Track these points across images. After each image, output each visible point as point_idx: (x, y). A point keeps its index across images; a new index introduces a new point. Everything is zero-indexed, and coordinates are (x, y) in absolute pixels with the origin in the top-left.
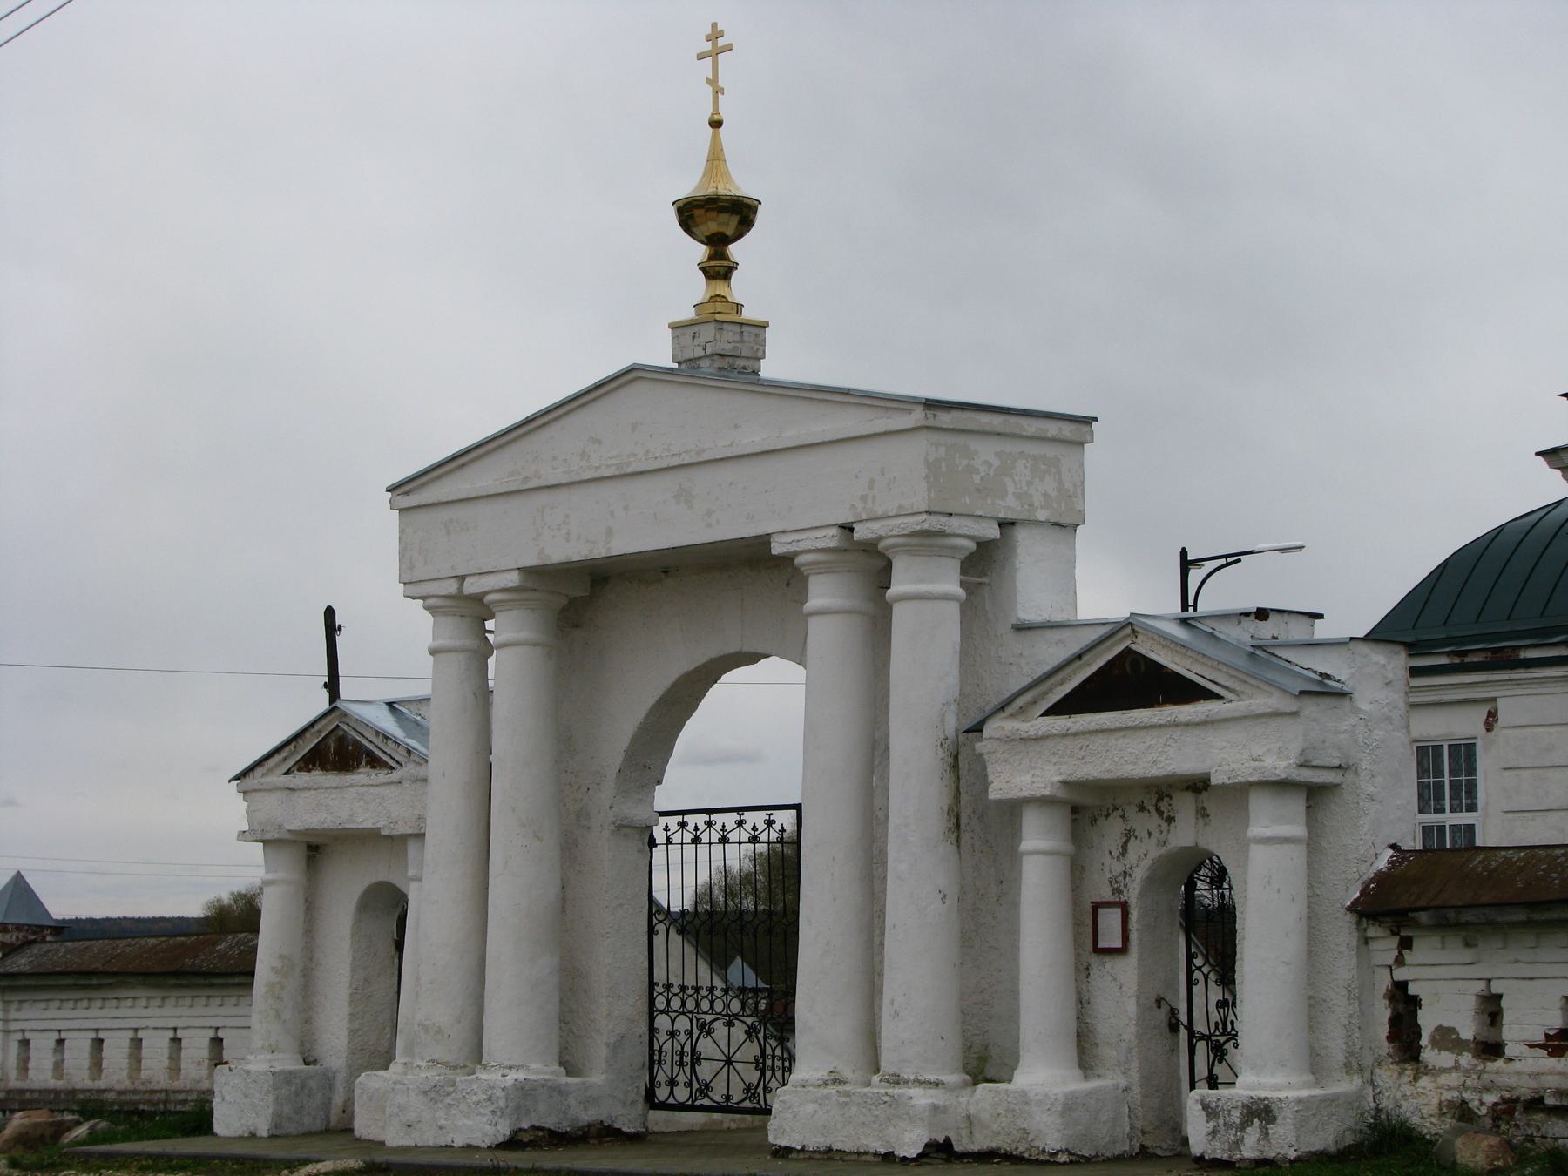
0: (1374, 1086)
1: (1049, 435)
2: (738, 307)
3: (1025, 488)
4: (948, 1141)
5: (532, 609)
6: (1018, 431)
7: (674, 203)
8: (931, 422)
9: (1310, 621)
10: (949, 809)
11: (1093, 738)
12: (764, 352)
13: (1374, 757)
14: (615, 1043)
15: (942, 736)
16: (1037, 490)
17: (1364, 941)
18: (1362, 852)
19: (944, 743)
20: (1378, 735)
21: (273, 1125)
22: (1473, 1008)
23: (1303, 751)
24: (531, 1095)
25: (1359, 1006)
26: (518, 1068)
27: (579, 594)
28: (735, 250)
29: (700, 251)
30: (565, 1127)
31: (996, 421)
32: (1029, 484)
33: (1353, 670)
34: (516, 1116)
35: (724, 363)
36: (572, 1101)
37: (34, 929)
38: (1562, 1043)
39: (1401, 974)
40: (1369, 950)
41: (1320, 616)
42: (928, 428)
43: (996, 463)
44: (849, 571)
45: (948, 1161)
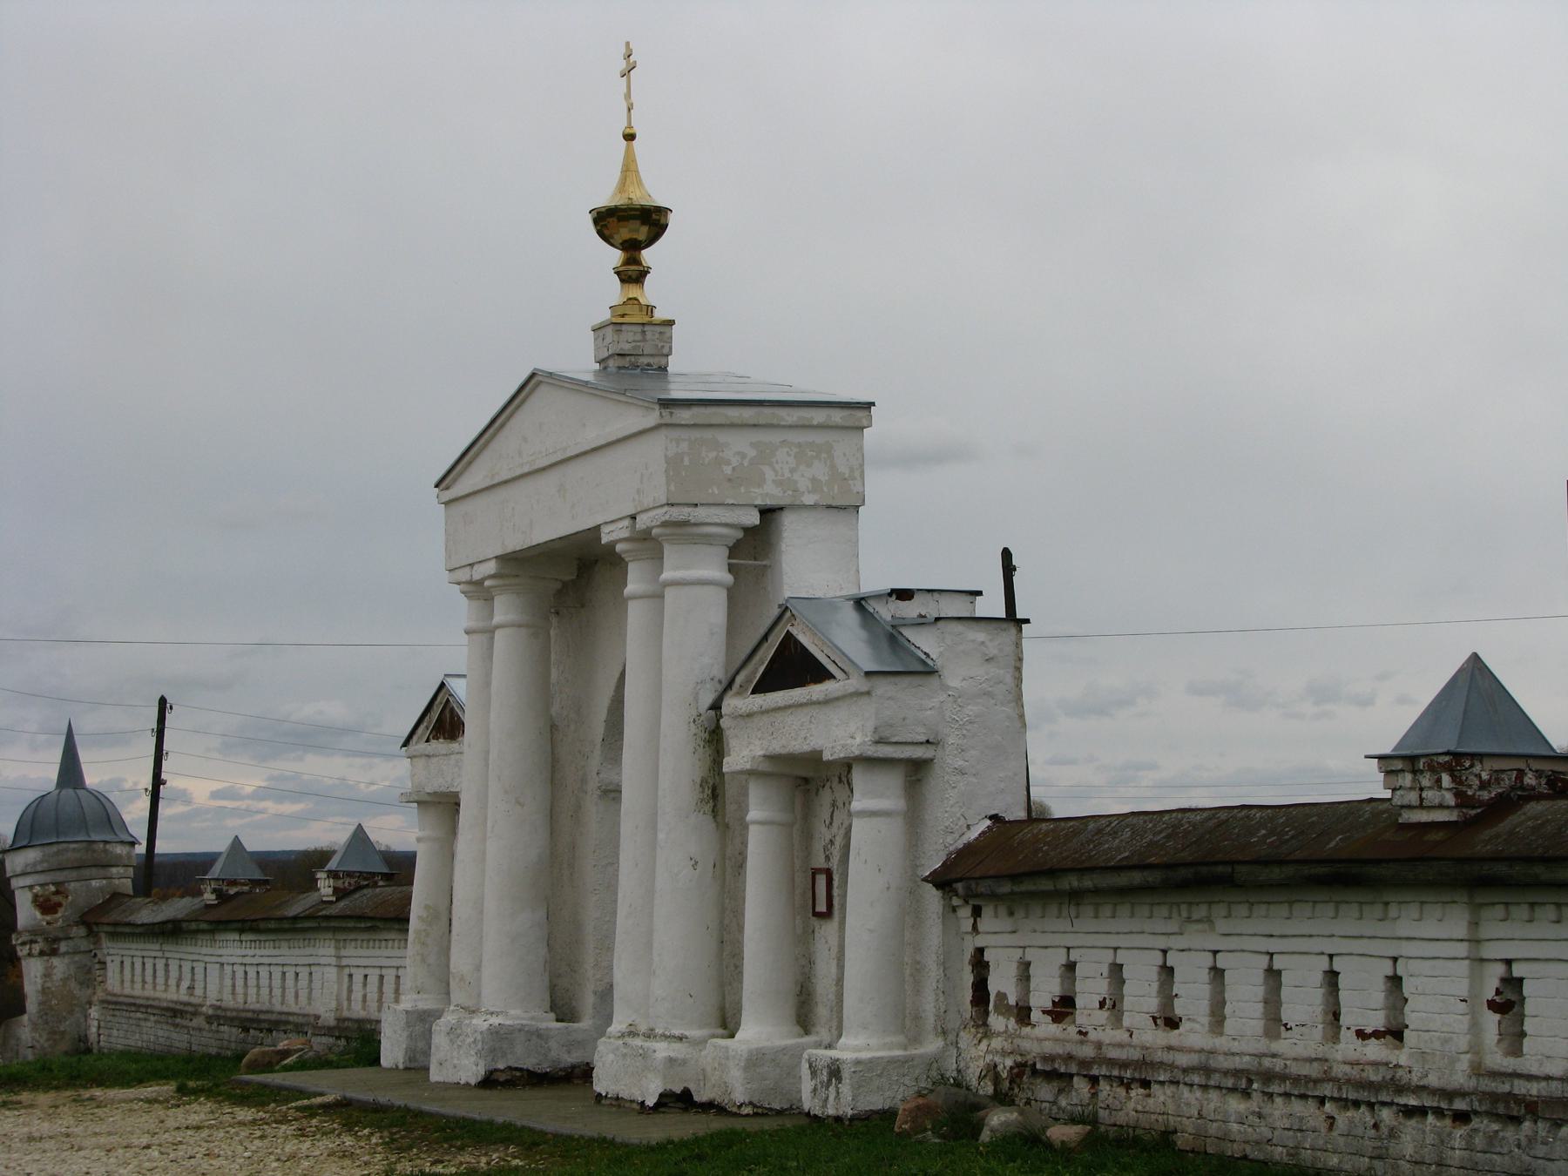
0: (958, 1048)
1: (815, 423)
2: (650, 309)
3: (787, 475)
4: (687, 1094)
5: (518, 593)
6: (775, 422)
7: (590, 212)
8: (667, 420)
9: (970, 598)
10: (702, 781)
11: (777, 715)
12: (671, 348)
13: (965, 732)
14: (602, 991)
15: (695, 713)
16: (803, 476)
17: (951, 910)
18: (947, 824)
19: (697, 719)
20: (971, 710)
21: (407, 1058)
22: (1014, 975)
23: (876, 728)
24: (507, 1038)
25: (944, 971)
26: (498, 1014)
27: (567, 578)
28: (648, 256)
29: (615, 256)
30: (545, 1067)
31: (747, 414)
32: (792, 471)
33: (942, 649)
34: (491, 1057)
35: (626, 362)
36: (553, 1044)
37: (365, 875)
38: (1063, 1010)
39: (980, 941)
40: (957, 918)
41: (979, 593)
42: (667, 425)
43: (752, 453)
44: (653, 558)
45: (686, 1110)
